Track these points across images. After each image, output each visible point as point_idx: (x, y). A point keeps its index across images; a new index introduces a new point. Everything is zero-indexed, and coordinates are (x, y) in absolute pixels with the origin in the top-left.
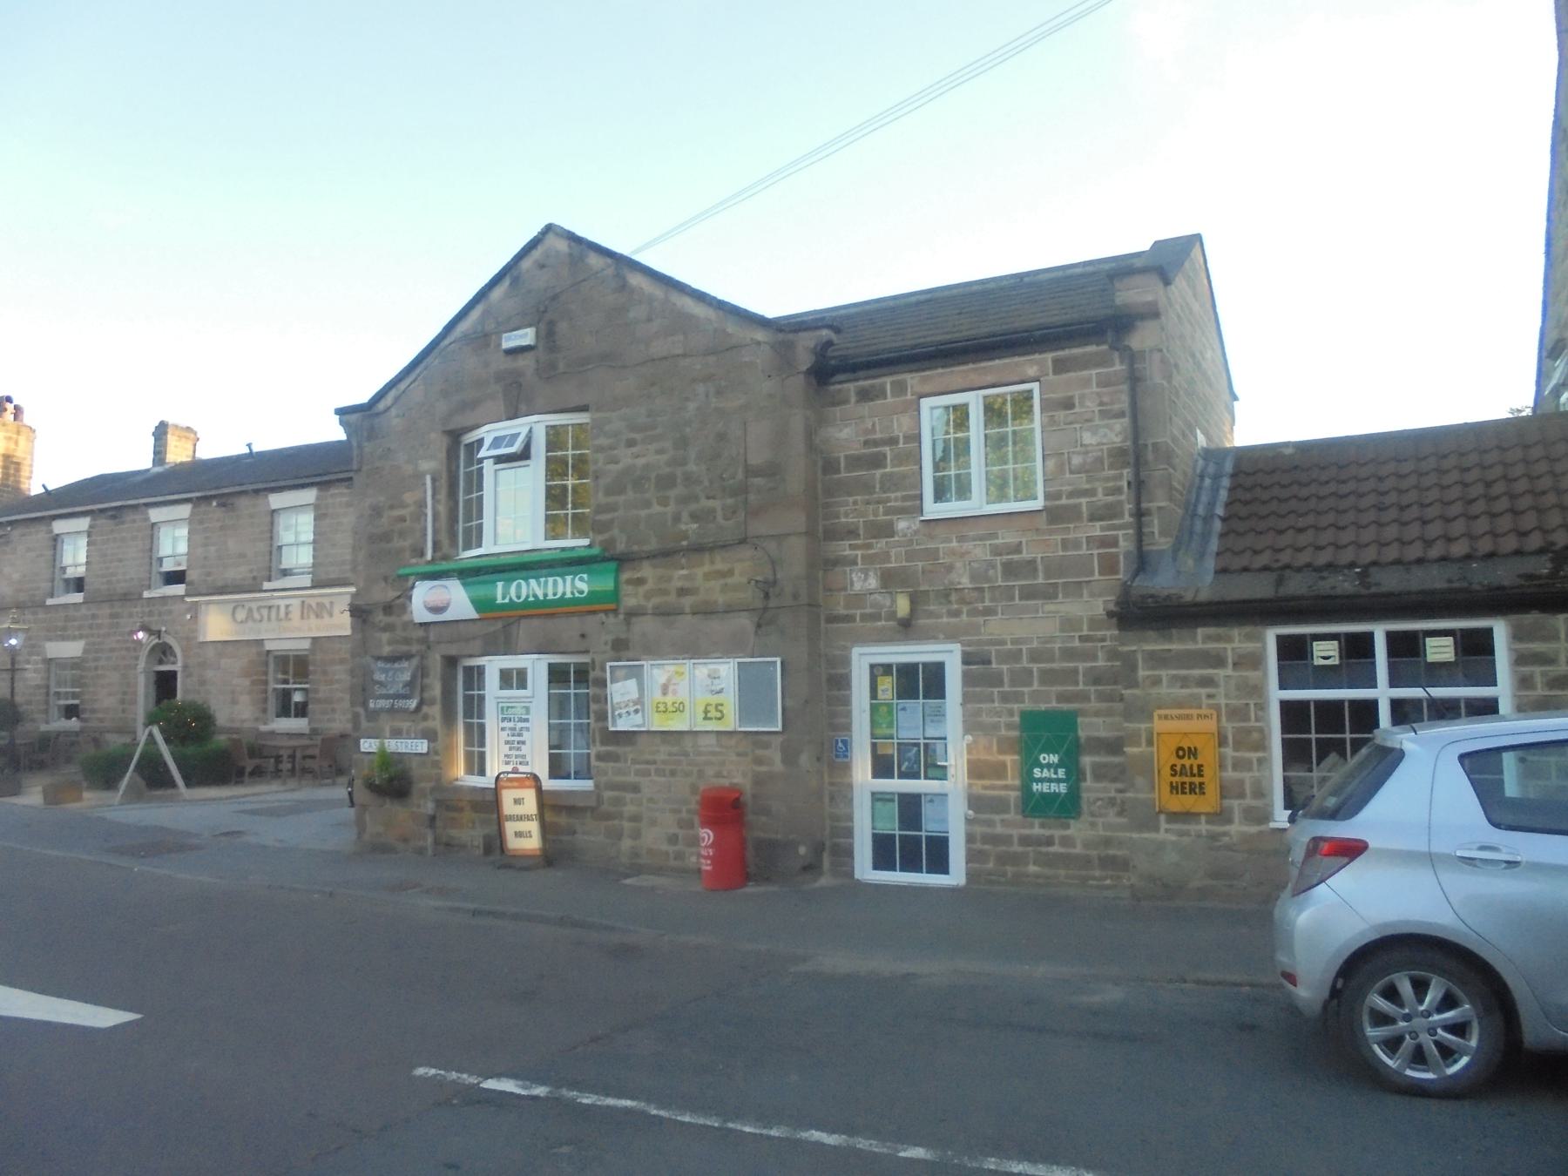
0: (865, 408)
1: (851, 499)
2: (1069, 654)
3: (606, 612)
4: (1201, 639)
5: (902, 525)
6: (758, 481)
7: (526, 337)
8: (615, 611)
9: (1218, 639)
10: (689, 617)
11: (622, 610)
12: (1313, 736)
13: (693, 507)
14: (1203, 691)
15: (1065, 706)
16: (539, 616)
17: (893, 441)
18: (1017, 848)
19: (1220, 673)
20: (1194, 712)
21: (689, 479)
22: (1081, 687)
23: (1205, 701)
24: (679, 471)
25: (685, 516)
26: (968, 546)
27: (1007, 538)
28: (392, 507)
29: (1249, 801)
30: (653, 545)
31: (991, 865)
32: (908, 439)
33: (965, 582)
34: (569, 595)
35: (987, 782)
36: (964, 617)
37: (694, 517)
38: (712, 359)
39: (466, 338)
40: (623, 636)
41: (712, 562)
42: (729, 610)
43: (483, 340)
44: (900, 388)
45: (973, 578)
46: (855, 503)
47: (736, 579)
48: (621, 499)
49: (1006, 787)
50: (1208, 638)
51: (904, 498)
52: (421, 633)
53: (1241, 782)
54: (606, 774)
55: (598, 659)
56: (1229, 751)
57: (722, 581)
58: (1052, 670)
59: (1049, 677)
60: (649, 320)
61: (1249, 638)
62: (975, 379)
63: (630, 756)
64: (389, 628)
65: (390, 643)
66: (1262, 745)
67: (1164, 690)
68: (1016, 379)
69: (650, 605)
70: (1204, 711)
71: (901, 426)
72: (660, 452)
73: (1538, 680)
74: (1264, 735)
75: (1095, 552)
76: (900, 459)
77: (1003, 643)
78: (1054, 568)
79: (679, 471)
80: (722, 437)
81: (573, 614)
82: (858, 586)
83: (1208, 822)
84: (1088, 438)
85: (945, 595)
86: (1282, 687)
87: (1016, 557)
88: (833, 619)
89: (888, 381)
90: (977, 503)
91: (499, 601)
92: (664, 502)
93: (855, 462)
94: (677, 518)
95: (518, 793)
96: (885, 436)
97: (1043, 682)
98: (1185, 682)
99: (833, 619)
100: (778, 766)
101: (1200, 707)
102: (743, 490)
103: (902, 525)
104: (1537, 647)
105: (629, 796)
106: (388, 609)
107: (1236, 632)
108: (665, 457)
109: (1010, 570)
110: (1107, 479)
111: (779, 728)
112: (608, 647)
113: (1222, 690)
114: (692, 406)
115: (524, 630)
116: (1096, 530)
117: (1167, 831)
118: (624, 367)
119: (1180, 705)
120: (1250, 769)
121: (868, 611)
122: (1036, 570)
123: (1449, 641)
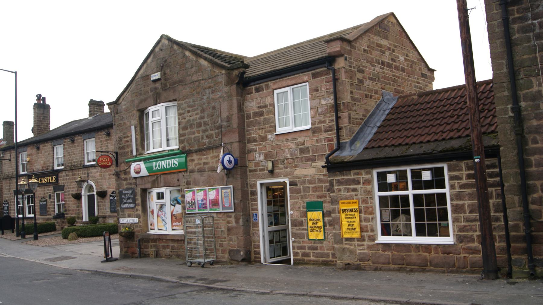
3: (184, 171)
4: (352, 176)
7: (156, 76)
8: (186, 171)
9: (357, 174)
12: (425, 208)
14: (354, 193)
17: (266, 106)
18: (307, 251)
20: (352, 201)
21: (206, 124)
22: (324, 192)
23: (355, 197)
25: (205, 138)
26: (289, 143)
27: (301, 140)
28: (125, 137)
30: (196, 148)
32: (270, 105)
34: (173, 166)
35: (298, 228)
41: (213, 153)
44: (267, 87)
45: (291, 154)
46: (256, 129)
48: (187, 131)
49: (303, 229)
50: (355, 174)
51: (270, 127)
53: (367, 226)
55: (183, 188)
56: (363, 215)
59: (315, 189)
60: (192, 68)
61: (367, 173)
64: (126, 179)
67: (343, 193)
68: (301, 81)
70: (355, 201)
71: (269, 100)
72: (197, 114)
73: (456, 185)
74: (373, 208)
75: (326, 143)
76: (269, 113)
79: (202, 121)
81: (175, 173)
83: (358, 241)
86: (379, 191)
87: (303, 146)
88: (251, 171)
89: (264, 84)
92: (198, 132)
93: (256, 114)
94: (202, 138)
96: (264, 105)
98: (348, 190)
99: (251, 171)
101: (353, 199)
103: (270, 136)
104: (457, 173)
107: (363, 171)
108: (198, 116)
111: (233, 211)
113: (359, 192)
114: (205, 97)
115: (162, 179)
116: (326, 135)
117: (346, 244)
118: (186, 85)
119: (347, 199)
120: (369, 222)
121: (261, 167)
122: (309, 151)
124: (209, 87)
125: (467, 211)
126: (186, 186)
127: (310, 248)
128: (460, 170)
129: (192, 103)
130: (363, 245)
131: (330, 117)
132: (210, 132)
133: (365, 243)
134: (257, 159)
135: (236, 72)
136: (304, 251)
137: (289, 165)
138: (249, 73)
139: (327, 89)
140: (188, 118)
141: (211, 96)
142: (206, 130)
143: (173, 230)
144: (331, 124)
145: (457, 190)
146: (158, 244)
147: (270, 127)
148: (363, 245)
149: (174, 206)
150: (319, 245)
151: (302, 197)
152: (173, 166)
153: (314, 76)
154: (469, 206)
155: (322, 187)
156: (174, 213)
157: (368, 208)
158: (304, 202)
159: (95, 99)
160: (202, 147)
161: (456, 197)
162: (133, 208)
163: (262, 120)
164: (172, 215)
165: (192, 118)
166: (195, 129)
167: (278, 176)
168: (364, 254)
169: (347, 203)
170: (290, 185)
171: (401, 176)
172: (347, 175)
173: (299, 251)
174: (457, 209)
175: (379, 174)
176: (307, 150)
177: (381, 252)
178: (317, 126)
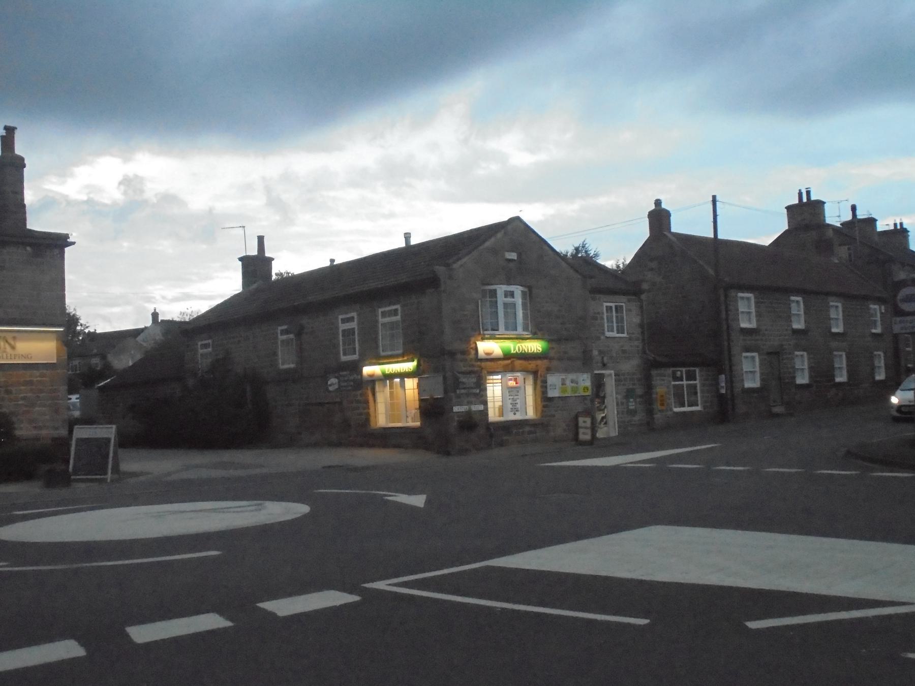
7: (513, 256)
153: (629, 301)
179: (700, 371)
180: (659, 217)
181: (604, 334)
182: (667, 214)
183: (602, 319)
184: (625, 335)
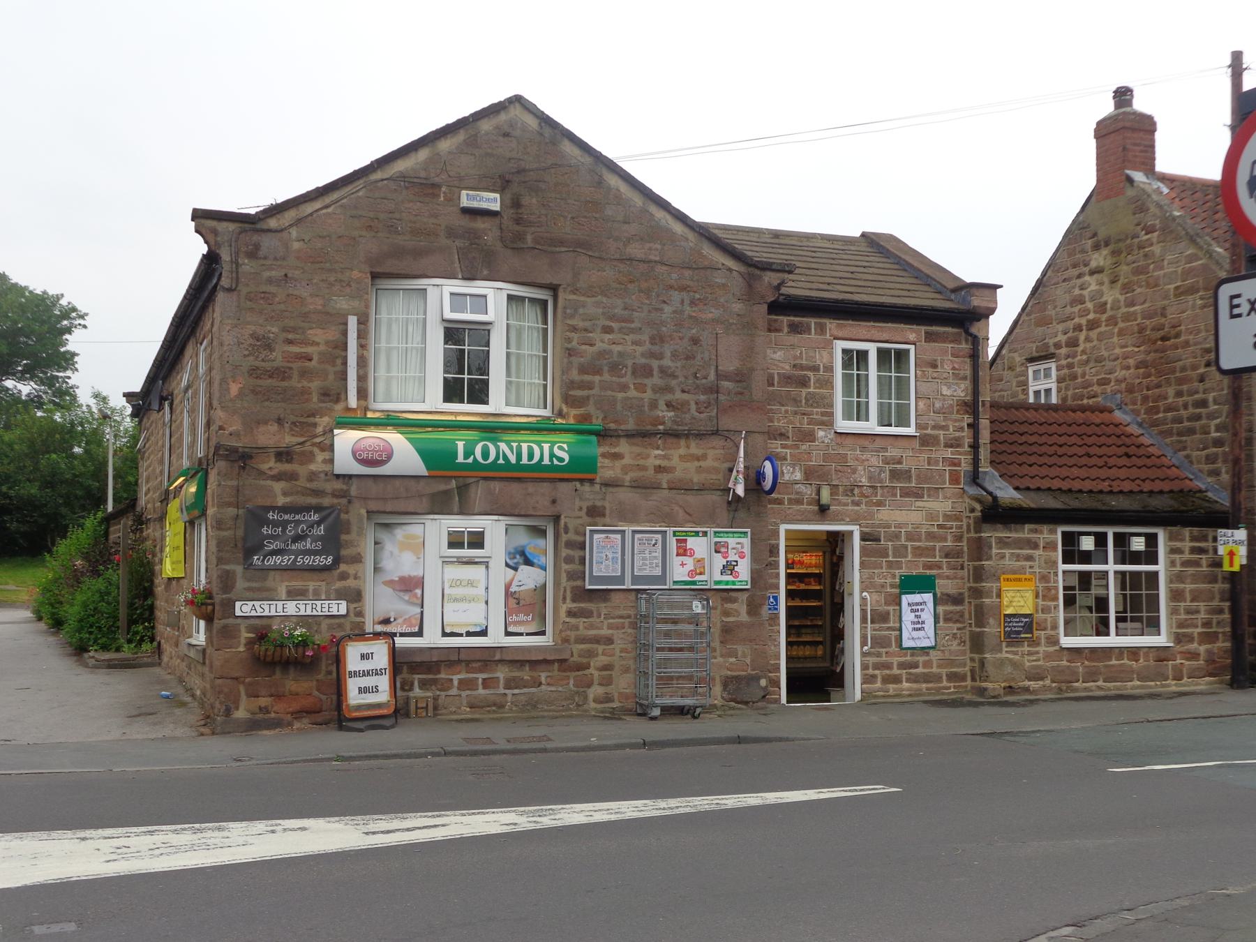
0: (794, 339)
1: (783, 409)
2: (931, 536)
3: (582, 481)
4: (1026, 532)
5: (821, 434)
6: (726, 384)
7: (491, 201)
8: (591, 481)
9: (1036, 531)
10: (666, 492)
11: (598, 480)
13: (669, 397)
14: (1028, 563)
15: (928, 572)
16: (502, 479)
17: (815, 369)
18: (896, 671)
19: (1036, 553)
20: (1023, 577)
24: (655, 364)
26: (866, 456)
27: (893, 452)
29: (1049, 632)
30: (631, 425)
31: (879, 685)
33: (864, 481)
34: (546, 461)
36: (863, 506)
37: (669, 405)
38: (687, 273)
39: (403, 179)
40: (599, 504)
41: (688, 447)
42: (702, 489)
43: (425, 187)
44: (821, 329)
45: (870, 478)
46: (786, 412)
47: (709, 463)
49: (889, 629)
50: (1031, 531)
51: (823, 414)
52: (338, 485)
54: (577, 628)
57: (696, 464)
58: (919, 547)
59: (919, 552)
62: (876, 334)
63: (604, 611)
65: (285, 494)
66: (1056, 598)
69: (628, 478)
70: (1027, 576)
77: (889, 527)
78: (923, 477)
79: (655, 364)
80: (695, 341)
82: (787, 477)
84: (945, 391)
85: (850, 491)
87: (898, 466)
90: (871, 425)
91: (460, 459)
92: (641, 388)
93: (787, 379)
94: (654, 405)
95: (364, 647)
97: (915, 555)
100: (744, 617)
102: (716, 390)
103: (821, 434)
104: (1178, 544)
105: (600, 648)
106: (284, 455)
108: (640, 349)
109: (895, 475)
110: (956, 421)
112: (583, 513)
115: (478, 493)
116: (948, 453)
122: (910, 477)
123: (1142, 539)
124: (683, 289)
125: (1188, 598)
126: (589, 520)
127: (902, 666)
128: (1183, 540)
129: (618, 311)
130: (1037, 653)
131: (956, 421)
132: (679, 395)
133: (1042, 649)
134: (787, 477)
135: (771, 278)
136: (888, 672)
137: (864, 500)
138: (797, 287)
139: (954, 368)
140: (600, 346)
141: (688, 310)
142: (668, 389)
143: (508, 634)
144: (957, 434)
145: (1179, 568)
146: (442, 676)
147: (823, 414)
148: (1037, 653)
149: (516, 569)
150: (921, 659)
151: (890, 565)
152: (546, 461)
153: (930, 337)
154: (1191, 591)
155: (934, 548)
156: (513, 589)
157: (1049, 589)
158: (894, 576)
159: (247, 196)
160: (649, 427)
161: (1176, 578)
162: (326, 569)
163: (804, 395)
164: (508, 594)
165: (616, 348)
166: (628, 379)
167: (838, 519)
168: (1038, 667)
169: (1015, 580)
170: (863, 539)
171: (1101, 540)
172: (1016, 531)
173: (877, 672)
174: (1176, 596)
175: (1065, 535)
176: (907, 475)
177: (1065, 663)
178: (929, 431)
179: (1171, 538)
180: (1125, 136)
181: (828, 423)
182: (1146, 126)
183: (829, 383)
184: (911, 430)
